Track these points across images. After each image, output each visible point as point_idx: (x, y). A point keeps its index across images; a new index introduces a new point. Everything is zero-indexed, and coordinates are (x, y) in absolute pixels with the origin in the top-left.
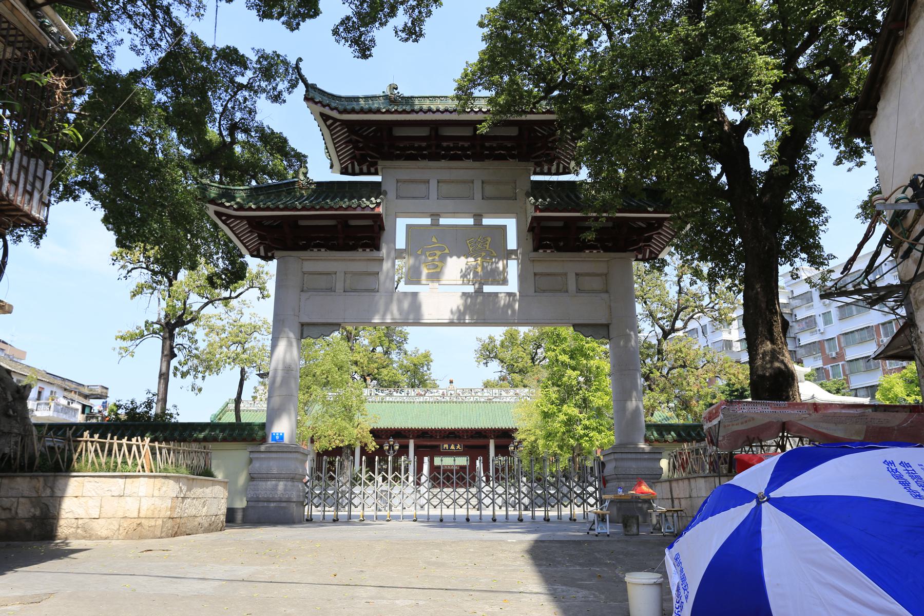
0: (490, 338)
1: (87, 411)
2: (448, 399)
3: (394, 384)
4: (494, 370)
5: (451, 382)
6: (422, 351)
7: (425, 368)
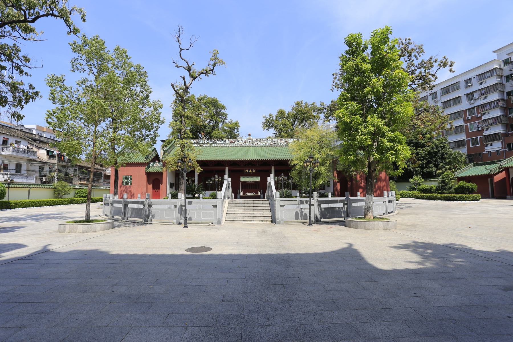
0: (270, 115)
1: (50, 154)
2: (248, 144)
3: (220, 138)
4: (272, 132)
5: (249, 135)
6: (234, 122)
7: (236, 130)
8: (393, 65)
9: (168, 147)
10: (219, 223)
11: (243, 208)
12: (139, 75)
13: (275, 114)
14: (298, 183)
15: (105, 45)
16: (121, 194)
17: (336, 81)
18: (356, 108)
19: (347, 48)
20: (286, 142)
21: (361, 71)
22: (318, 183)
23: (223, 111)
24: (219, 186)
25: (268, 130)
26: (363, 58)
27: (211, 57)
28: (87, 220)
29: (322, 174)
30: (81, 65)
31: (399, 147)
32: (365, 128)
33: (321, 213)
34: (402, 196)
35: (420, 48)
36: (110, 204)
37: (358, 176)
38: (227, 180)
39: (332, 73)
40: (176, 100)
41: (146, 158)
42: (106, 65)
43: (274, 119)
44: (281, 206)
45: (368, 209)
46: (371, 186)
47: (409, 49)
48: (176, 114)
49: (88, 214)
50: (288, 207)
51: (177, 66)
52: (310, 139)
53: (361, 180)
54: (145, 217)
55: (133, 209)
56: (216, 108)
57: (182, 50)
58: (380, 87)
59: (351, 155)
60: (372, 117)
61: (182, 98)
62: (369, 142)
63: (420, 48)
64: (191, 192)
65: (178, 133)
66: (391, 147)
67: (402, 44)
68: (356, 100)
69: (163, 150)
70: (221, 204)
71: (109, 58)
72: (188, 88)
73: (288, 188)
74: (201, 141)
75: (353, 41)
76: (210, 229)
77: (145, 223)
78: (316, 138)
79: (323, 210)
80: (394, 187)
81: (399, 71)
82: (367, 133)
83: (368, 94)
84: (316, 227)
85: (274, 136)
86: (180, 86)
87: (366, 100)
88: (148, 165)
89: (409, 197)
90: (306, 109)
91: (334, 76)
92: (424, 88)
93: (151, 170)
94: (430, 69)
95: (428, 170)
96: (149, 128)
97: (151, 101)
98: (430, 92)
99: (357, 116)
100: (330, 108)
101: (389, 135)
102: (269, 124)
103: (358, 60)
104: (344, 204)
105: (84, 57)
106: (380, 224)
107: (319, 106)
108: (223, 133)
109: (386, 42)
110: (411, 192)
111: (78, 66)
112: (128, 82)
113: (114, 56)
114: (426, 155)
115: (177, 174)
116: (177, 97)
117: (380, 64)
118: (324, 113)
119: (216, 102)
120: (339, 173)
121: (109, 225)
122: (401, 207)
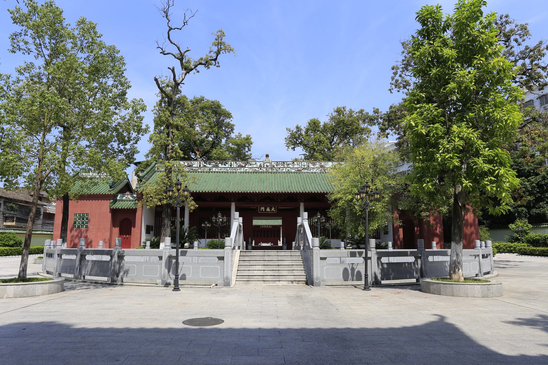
0: (297, 127)
2: (264, 170)
3: (223, 160)
4: (300, 151)
5: (267, 156)
6: (244, 136)
8: (490, 51)
9: (145, 172)
10: (227, 284)
11: (262, 263)
12: (112, 61)
13: (304, 125)
14: (340, 228)
15: (64, 15)
16: (71, 241)
17: (397, 77)
18: (435, 113)
19: (419, 27)
20: (322, 166)
21: (442, 60)
22: (371, 228)
23: (227, 120)
24: (226, 231)
25: (293, 149)
26: (444, 40)
27: (214, 40)
28: (22, 278)
29: (377, 213)
30: (26, 43)
31: (502, 171)
32: (449, 142)
33: (383, 270)
34: (500, 250)
35: (524, 28)
36: (56, 256)
37: (431, 219)
38: (237, 222)
39: (391, 66)
40: (161, 101)
41: (111, 187)
42: (64, 46)
43: (303, 133)
44: (322, 259)
45: (455, 266)
46: (451, 232)
47: (507, 30)
48: (158, 123)
49: (24, 270)
50: (333, 261)
51: (163, 53)
52: (359, 163)
53: (437, 224)
54: (112, 275)
55: (94, 262)
56: (217, 115)
57: (171, 29)
58: (471, 82)
59: (428, 182)
60: (459, 127)
61: (170, 99)
62: (456, 162)
63: (524, 28)
64: (180, 241)
65: (162, 150)
66: (489, 170)
67: (496, 23)
68: (435, 102)
69: (138, 176)
70: (230, 255)
71: (69, 34)
72: (178, 84)
73: (329, 234)
74: (196, 164)
75: (429, 16)
76: (215, 293)
77: (113, 283)
78: (368, 161)
79: (385, 266)
80: (486, 236)
81: (499, 59)
82: (452, 150)
83: (452, 92)
84: (375, 291)
85: (303, 157)
86: (167, 81)
87: (449, 101)
88: (113, 198)
89: (510, 252)
90: (350, 119)
91: (394, 71)
92: (530, 88)
93: (118, 205)
94: (539, 59)
95: (538, 211)
96: (123, 139)
97: (129, 101)
98: (541, 93)
99: (436, 125)
100: (388, 117)
101: (486, 153)
102: (295, 140)
103: (436, 44)
104: (417, 258)
105: (30, 32)
106: (476, 288)
107: (371, 113)
108: (227, 153)
109: (477, 18)
110: (512, 245)
111: (21, 44)
112: (96, 71)
113: (76, 32)
114: (533, 188)
115: (159, 213)
116: (163, 98)
117: (470, 51)
118: (379, 124)
119: (219, 106)
120: (403, 214)
121: (56, 286)
122: (503, 266)
